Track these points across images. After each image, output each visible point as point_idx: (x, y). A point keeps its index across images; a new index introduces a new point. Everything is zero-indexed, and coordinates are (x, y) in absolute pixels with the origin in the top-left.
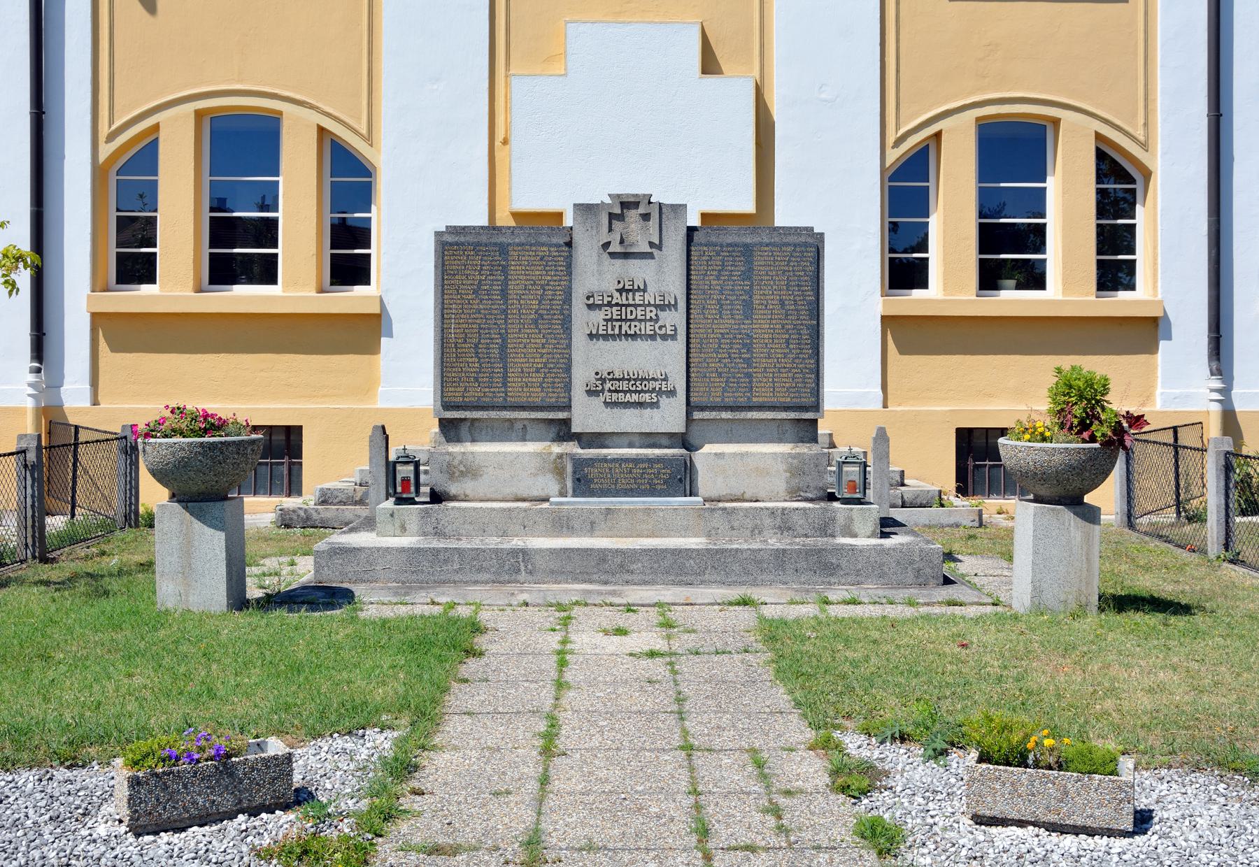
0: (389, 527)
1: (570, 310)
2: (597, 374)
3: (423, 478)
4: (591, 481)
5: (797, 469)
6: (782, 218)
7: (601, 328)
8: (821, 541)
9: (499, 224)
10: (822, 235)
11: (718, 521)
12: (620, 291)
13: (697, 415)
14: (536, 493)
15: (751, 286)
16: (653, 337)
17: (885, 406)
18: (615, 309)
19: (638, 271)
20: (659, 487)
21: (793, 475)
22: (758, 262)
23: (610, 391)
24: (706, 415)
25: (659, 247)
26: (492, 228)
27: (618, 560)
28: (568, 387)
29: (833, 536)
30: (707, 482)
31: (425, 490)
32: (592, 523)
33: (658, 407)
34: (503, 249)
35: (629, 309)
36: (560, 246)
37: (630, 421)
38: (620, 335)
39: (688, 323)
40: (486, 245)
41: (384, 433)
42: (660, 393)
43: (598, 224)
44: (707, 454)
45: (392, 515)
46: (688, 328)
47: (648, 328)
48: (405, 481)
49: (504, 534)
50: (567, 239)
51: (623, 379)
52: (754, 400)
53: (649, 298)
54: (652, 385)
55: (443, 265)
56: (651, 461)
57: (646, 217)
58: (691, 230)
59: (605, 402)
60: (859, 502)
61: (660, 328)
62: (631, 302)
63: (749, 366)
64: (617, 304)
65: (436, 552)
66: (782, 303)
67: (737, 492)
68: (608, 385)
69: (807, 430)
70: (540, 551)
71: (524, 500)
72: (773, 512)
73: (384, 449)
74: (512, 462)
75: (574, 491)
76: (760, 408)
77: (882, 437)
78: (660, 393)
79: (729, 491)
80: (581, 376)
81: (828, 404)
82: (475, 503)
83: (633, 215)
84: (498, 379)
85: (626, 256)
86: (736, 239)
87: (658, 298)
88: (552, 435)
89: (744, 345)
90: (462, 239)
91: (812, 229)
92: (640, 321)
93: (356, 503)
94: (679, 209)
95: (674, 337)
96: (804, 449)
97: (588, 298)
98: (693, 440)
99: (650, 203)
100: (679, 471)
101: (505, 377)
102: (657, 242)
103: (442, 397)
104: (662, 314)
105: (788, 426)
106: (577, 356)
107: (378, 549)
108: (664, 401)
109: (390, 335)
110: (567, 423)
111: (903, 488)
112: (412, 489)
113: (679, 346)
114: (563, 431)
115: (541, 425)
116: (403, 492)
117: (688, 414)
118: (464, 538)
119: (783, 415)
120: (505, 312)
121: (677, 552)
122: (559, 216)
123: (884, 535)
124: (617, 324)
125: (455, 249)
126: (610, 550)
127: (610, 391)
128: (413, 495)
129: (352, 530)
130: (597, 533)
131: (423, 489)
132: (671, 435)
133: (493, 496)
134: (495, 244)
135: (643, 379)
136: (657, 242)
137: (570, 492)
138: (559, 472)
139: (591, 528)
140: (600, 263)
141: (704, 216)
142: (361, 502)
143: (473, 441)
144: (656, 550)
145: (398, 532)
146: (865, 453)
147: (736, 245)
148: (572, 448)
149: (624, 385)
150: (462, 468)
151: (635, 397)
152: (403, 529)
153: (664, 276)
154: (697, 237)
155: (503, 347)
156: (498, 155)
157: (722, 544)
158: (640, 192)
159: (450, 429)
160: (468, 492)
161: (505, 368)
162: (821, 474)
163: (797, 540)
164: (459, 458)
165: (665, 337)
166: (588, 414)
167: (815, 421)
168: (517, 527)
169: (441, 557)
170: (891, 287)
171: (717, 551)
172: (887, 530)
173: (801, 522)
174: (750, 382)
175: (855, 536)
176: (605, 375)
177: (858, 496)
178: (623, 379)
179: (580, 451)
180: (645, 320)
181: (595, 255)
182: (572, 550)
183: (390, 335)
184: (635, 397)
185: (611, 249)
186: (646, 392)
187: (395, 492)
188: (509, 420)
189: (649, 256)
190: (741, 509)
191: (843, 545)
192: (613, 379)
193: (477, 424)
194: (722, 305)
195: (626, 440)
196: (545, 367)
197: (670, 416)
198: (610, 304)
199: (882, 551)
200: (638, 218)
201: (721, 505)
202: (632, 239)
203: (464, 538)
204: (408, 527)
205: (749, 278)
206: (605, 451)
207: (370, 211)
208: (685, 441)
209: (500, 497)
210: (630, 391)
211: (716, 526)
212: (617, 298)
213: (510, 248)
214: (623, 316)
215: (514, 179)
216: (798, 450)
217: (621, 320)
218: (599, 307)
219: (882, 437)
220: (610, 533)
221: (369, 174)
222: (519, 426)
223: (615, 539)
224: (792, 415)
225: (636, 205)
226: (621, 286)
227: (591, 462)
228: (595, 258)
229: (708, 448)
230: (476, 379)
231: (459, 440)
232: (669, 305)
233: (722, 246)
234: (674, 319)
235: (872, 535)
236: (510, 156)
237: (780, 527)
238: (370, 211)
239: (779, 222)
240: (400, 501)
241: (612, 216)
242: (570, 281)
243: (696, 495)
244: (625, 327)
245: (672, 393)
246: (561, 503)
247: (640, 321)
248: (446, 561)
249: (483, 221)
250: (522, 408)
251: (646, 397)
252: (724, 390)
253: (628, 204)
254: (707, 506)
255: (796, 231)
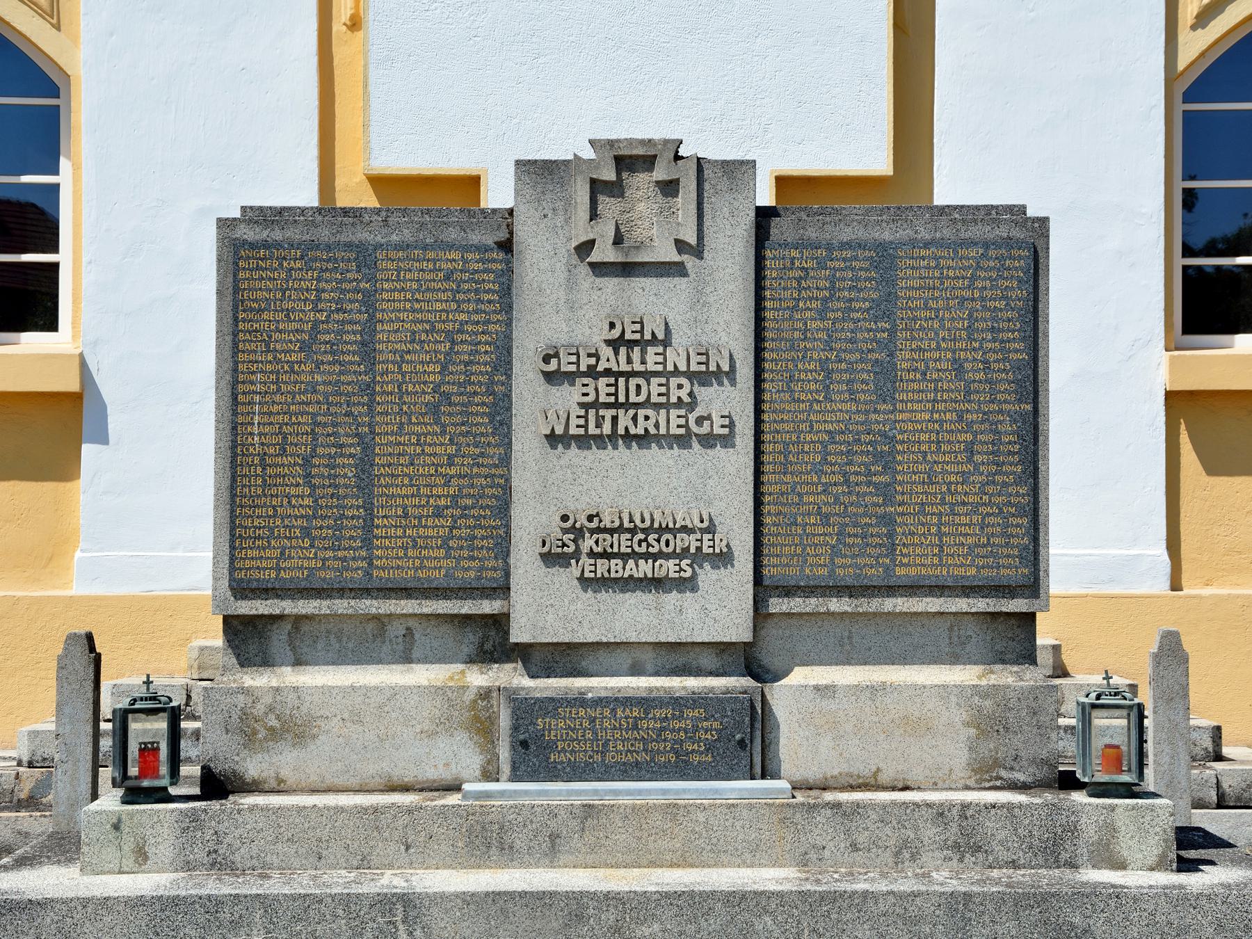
0: (110, 854)
1: (508, 384)
2: (565, 518)
3: (187, 748)
4: (551, 746)
5: (992, 720)
6: (949, 188)
7: (574, 421)
8: (1047, 877)
9: (342, 201)
10: (1044, 222)
11: (822, 831)
12: (615, 344)
13: (777, 605)
14: (432, 773)
15: (892, 332)
16: (683, 441)
17: (1176, 586)
18: (602, 382)
19: (651, 301)
20: (696, 759)
21: (983, 733)
22: (908, 280)
23: (592, 554)
24: (796, 604)
25: (698, 251)
26: (327, 210)
27: (610, 917)
28: (503, 547)
29: (1073, 866)
30: (798, 748)
31: (191, 771)
32: (554, 837)
33: (694, 589)
34: (365, 257)
35: (633, 382)
36: (487, 249)
37: (635, 617)
38: (613, 437)
39: (758, 412)
40: (329, 248)
41: (92, 648)
42: (698, 557)
43: (569, 203)
44: (796, 689)
45: (116, 827)
46: (758, 422)
47: (673, 422)
48: (148, 751)
49: (364, 863)
50: (502, 235)
51: (620, 529)
52: (900, 571)
53: (675, 358)
54: (682, 541)
55: (236, 290)
56: (678, 703)
57: (669, 188)
58: (764, 215)
59: (582, 579)
60: (1129, 791)
61: (700, 421)
62: (638, 367)
63: (889, 500)
64: (608, 373)
65: (214, 904)
66: (958, 368)
67: (863, 769)
68: (588, 543)
69: (1014, 637)
70: (441, 899)
71: (406, 789)
72: (940, 813)
73: (89, 686)
74: (384, 709)
75: (514, 768)
76: (913, 589)
77: (1171, 653)
78: (698, 557)
79: (844, 768)
80: (531, 522)
81: (1058, 582)
82: (298, 794)
83: (641, 184)
84: (352, 530)
85: (627, 269)
86: (861, 234)
87: (695, 359)
88: (466, 650)
89: (878, 456)
90: (277, 235)
91: (1022, 209)
92: (658, 406)
93: (19, 805)
94: (739, 171)
95: (727, 441)
96: (1006, 677)
97: (546, 359)
98: (769, 657)
99: (677, 158)
100: (738, 725)
101: (369, 526)
102: (693, 240)
103: (232, 569)
104: (702, 393)
105: (971, 629)
106: (524, 480)
107: (85, 902)
108: (707, 576)
109: (103, 439)
110: (500, 622)
111: (1219, 766)
112: (164, 769)
113: (739, 459)
114: (492, 641)
115: (446, 629)
116: (143, 774)
117: (759, 603)
118: (275, 874)
119: (961, 604)
120: (369, 389)
121: (737, 899)
122: (472, 183)
123: (1186, 866)
124: (608, 414)
125: (256, 252)
126: (593, 895)
127: (592, 554)
128: (164, 782)
129: (22, 863)
130: (564, 858)
131: (185, 770)
132: (722, 648)
133: (340, 781)
134: (349, 246)
135: (662, 530)
136: (693, 240)
137: (506, 769)
138: (483, 728)
139: (552, 848)
140: (571, 284)
141: (783, 182)
142: (31, 803)
143: (298, 662)
144: (692, 894)
145: (129, 863)
146: (1133, 688)
147: (861, 245)
148: (511, 676)
149: (623, 543)
150: (273, 722)
151: (645, 568)
152: (141, 855)
153: (709, 312)
154: (778, 229)
155: (365, 464)
156: (340, 53)
157: (833, 882)
158: (657, 135)
159: (247, 638)
160: (285, 773)
161: (369, 507)
162: (1045, 729)
163: (995, 873)
164: (268, 699)
165: (708, 441)
166: (544, 605)
167: (1030, 617)
168: (393, 847)
169: (225, 916)
170: (1186, 331)
171: (823, 897)
172: (1192, 854)
173: (1001, 835)
174: (891, 535)
175: (1122, 866)
176: (582, 520)
177: (1125, 778)
178: (620, 529)
179: (527, 682)
180: (667, 406)
181: (560, 267)
182: (511, 895)
183: (103, 439)
184: (645, 568)
185: (595, 257)
186: (668, 557)
187: (125, 776)
188: (377, 618)
189: (678, 270)
190: (872, 806)
191: (1096, 885)
192: (599, 530)
193: (305, 627)
194: (829, 373)
195: (625, 659)
196: (455, 505)
197: (719, 608)
198: (592, 372)
199: (1182, 899)
200: (653, 191)
201: (829, 796)
202: (639, 233)
203: (275, 874)
204: (151, 850)
205: (888, 315)
206: (580, 683)
207: (56, 172)
208: (750, 660)
209: (354, 782)
210: (635, 555)
211: (820, 842)
212: (608, 358)
213: (380, 255)
214: (620, 397)
215: (375, 104)
216: (993, 680)
217: (616, 405)
218: (570, 377)
219: (1171, 653)
220: (590, 859)
221: (53, 90)
222: (397, 629)
223: (601, 872)
224: (982, 605)
225: (648, 162)
226: (616, 333)
227: (551, 705)
228: (562, 276)
229: (800, 676)
230: (306, 532)
231: (266, 662)
232: (718, 375)
233: (829, 247)
234: (730, 402)
235: (1160, 865)
236: (366, 54)
237: (956, 846)
238: (56, 172)
239: (942, 197)
240: (135, 795)
241: (597, 187)
242: (509, 323)
243: (776, 776)
244: (624, 421)
245: (724, 558)
246: (487, 795)
247: (658, 406)
248: (235, 925)
249: (308, 197)
250: (406, 592)
251: (669, 568)
252: (835, 552)
253: (631, 160)
254: (800, 798)
255: (990, 213)
